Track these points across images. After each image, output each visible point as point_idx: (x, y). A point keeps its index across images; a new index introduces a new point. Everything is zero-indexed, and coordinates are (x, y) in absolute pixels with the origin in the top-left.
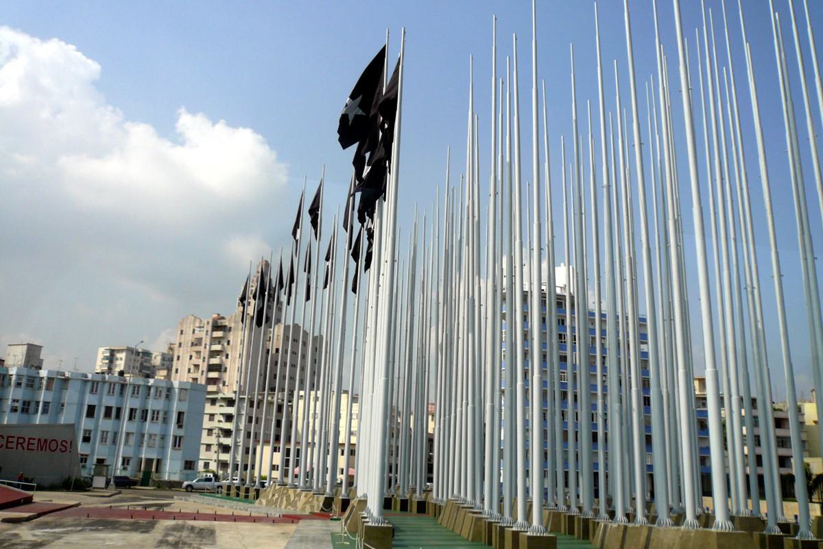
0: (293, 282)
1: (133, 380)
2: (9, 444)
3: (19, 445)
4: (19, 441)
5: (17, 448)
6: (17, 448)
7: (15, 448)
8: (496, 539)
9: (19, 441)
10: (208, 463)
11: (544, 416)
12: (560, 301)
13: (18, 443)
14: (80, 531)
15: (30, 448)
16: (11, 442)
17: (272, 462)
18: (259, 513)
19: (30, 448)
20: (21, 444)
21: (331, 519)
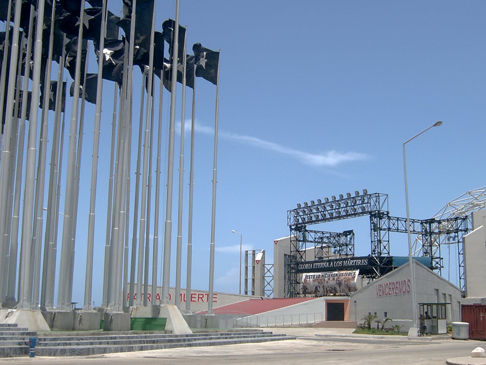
0: (41, 97)
1: (293, 237)
2: (193, 298)
3: (200, 299)
4: (200, 297)
5: (198, 301)
6: (198, 301)
7: (197, 301)
8: (362, 337)
9: (200, 297)
10: (462, 305)
11: (71, 266)
12: (52, 106)
13: (199, 298)
14: (56, 330)
15: (192, 300)
16: (194, 297)
17: (283, 299)
18: (309, 329)
19: (192, 300)
20: (201, 298)
21: (101, 324)
